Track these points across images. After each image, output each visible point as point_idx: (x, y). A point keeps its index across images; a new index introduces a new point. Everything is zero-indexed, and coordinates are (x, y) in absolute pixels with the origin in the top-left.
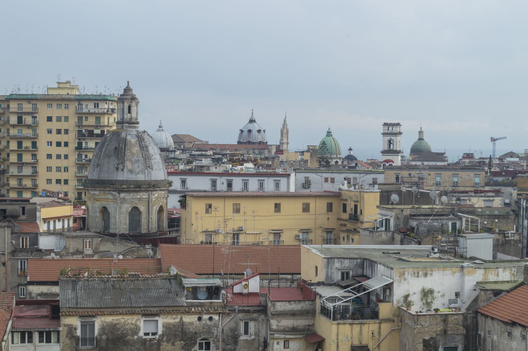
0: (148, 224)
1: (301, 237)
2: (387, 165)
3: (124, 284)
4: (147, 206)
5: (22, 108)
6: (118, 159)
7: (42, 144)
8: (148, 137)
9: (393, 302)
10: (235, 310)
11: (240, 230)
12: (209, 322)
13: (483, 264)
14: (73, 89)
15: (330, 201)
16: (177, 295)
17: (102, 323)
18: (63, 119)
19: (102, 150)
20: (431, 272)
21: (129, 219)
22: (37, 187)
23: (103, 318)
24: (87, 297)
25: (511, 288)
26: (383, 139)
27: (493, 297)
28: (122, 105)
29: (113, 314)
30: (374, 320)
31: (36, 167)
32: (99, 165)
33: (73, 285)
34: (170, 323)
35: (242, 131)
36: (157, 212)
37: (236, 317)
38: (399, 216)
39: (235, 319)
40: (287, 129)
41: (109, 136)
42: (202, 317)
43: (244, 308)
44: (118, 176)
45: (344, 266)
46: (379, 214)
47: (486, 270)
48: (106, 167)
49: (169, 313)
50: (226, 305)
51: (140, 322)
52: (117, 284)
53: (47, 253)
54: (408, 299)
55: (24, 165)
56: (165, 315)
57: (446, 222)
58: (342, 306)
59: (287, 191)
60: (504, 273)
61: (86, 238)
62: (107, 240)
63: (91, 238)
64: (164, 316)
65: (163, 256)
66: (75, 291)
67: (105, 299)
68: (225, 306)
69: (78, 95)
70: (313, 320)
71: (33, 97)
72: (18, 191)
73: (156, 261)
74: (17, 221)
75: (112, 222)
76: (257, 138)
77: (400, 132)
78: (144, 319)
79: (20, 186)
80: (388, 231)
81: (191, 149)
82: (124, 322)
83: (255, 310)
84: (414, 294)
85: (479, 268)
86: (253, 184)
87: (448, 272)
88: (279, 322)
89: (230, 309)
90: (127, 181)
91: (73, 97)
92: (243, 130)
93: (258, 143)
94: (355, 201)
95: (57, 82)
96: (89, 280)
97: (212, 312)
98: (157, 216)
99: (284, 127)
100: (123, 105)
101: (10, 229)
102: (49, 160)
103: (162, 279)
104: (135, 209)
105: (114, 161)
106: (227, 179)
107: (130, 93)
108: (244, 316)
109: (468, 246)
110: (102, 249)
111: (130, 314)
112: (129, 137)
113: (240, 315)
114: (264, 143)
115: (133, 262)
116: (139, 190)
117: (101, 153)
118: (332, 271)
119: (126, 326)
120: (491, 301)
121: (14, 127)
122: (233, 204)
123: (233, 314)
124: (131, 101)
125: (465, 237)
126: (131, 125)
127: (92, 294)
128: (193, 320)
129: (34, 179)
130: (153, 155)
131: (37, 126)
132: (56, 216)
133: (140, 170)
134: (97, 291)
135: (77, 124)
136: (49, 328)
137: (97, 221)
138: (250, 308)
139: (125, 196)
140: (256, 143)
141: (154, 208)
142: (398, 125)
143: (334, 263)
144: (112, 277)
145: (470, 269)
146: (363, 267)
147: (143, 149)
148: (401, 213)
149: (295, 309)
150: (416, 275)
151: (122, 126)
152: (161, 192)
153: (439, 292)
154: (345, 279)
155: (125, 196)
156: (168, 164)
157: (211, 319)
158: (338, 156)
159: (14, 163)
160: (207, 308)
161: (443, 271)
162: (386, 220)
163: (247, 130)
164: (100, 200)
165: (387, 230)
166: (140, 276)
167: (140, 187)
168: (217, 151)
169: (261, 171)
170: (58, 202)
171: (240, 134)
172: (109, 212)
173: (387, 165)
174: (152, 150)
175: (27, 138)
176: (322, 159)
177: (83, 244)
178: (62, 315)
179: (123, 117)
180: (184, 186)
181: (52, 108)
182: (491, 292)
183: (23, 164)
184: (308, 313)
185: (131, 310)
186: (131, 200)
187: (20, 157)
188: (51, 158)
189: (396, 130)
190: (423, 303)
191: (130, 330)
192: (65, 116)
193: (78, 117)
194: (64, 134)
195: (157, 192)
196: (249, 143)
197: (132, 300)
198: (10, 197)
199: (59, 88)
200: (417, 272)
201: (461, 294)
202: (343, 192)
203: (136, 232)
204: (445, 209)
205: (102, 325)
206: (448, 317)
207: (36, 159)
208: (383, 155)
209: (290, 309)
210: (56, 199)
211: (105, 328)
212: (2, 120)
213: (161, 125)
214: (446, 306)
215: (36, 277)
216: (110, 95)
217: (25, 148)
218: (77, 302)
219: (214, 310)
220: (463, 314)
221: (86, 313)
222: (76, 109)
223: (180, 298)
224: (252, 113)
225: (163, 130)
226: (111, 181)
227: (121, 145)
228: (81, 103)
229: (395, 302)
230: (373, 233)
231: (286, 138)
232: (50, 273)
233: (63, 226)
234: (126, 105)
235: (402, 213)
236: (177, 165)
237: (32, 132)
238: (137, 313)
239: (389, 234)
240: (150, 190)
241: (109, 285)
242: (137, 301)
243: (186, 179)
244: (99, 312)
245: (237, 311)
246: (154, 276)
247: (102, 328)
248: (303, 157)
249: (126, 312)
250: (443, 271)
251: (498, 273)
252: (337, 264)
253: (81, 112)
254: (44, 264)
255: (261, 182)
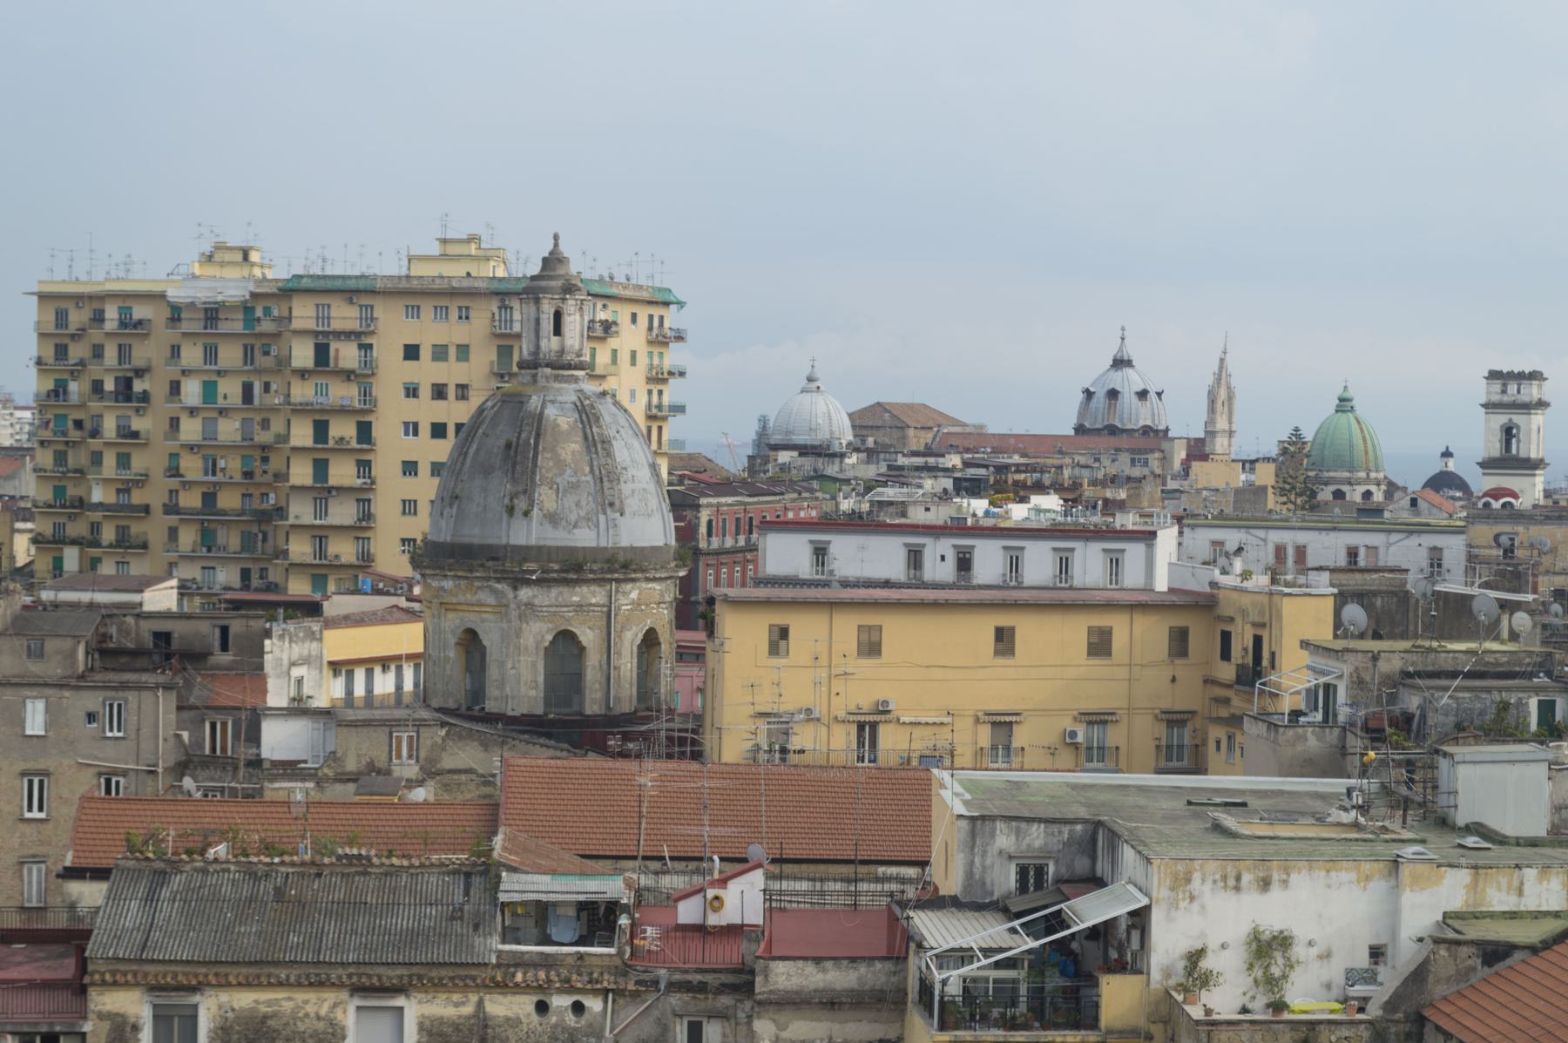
0: (604, 684)
1: (1080, 738)
2: (1496, 505)
3: (316, 887)
4: (605, 631)
5: (329, 318)
6: (514, 480)
7: (386, 430)
8: (614, 410)
9: (1148, 974)
10: (656, 982)
11: (882, 709)
12: (570, 1019)
13: (1489, 849)
14: (488, 259)
15: (1179, 621)
16: (476, 927)
17: (222, 1012)
18: (452, 352)
19: (468, 449)
20: (1284, 877)
21: (545, 671)
22: (373, 561)
23: (224, 997)
24: (185, 925)
25: (1544, 937)
26: (1487, 421)
27: (1480, 967)
28: (533, 308)
29: (256, 985)
30: (1083, 1032)
31: (369, 501)
32: (456, 497)
33: (154, 885)
34: (442, 1018)
35: (1089, 394)
36: (635, 649)
37: (660, 1006)
38: (1363, 675)
39: (656, 1013)
40: (1229, 388)
41: (493, 407)
42: (548, 1001)
43: (689, 977)
44: (511, 533)
45: (1029, 846)
46: (1309, 667)
47: (1477, 874)
48: (478, 504)
49: (438, 986)
50: (630, 966)
51: (345, 1012)
52: (294, 886)
53: (275, 772)
54: (1200, 964)
55: (334, 493)
56: (426, 992)
57: (1520, 699)
58: (995, 981)
59: (1146, 584)
60: (1545, 883)
61: (398, 728)
62: (464, 734)
63: (415, 729)
64: (423, 996)
65: (510, 795)
66: (150, 907)
67: (239, 931)
68: (624, 970)
69: (501, 279)
70: (898, 1025)
71: (361, 284)
72: (313, 575)
73: (484, 812)
74: (206, 669)
75: (494, 678)
76: (1137, 415)
77: (1540, 399)
78: (357, 1001)
79: (320, 559)
80: (1330, 724)
81: (892, 450)
82: (292, 1012)
83: (723, 985)
84: (1223, 946)
85: (1451, 866)
86: (1039, 563)
87: (1345, 875)
88: (782, 1027)
89: (641, 978)
90: (540, 548)
91: (482, 285)
92: (1092, 389)
93: (1138, 430)
94: (1254, 625)
95: (437, 239)
96: (208, 871)
97: (579, 985)
98: (635, 660)
99: (1219, 383)
100: (538, 309)
101: (173, 696)
102: (409, 480)
103: (444, 873)
104: (566, 639)
105: (501, 486)
106: (955, 546)
107: (561, 271)
108: (686, 1003)
109: (1460, 787)
110: (448, 762)
111: (311, 984)
112: (551, 412)
113: (675, 1000)
114: (1157, 432)
115: (412, 811)
116: (575, 577)
117: (464, 459)
118: (988, 862)
119: (299, 1023)
120: (1473, 980)
121: (303, 376)
122: (859, 626)
123: (652, 994)
124: (562, 296)
125: (1452, 755)
126: (562, 372)
127: (203, 917)
128: (520, 1011)
129: (363, 538)
130: (625, 469)
131: (373, 374)
132: (379, 655)
133: (582, 513)
134: (222, 908)
135: (496, 368)
136: (51, 1024)
137: (448, 672)
138: (708, 978)
139: (534, 596)
140: (1133, 430)
141: (628, 635)
142: (1535, 376)
143: (993, 835)
144: (282, 863)
145: (1420, 868)
146: (1094, 850)
147: (593, 450)
148: (1370, 665)
149: (838, 987)
150: (1231, 882)
151: (535, 376)
152: (650, 585)
153: (1310, 944)
154: (1032, 889)
155: (534, 596)
156: (800, 494)
157: (578, 1008)
158: (1373, 475)
159: (302, 489)
160: (564, 972)
161: (1328, 871)
162: (1327, 687)
163: (1105, 389)
164: (458, 607)
165: (1327, 722)
166: (375, 860)
167: (579, 568)
168: (976, 456)
169: (1082, 520)
170: (407, 611)
171: (1081, 403)
172: (485, 647)
173: (1496, 505)
174: (625, 450)
175: (343, 411)
176: (1289, 484)
177: (391, 746)
178: (93, 984)
179: (538, 347)
180: (823, 564)
181: (418, 317)
182: (1473, 950)
183: (330, 490)
184: (879, 1000)
185: (316, 971)
186: (552, 609)
187: (321, 468)
188: (416, 474)
189: (1532, 392)
190: (1256, 981)
191: (311, 1036)
192: (459, 343)
193: (498, 346)
194: (457, 399)
195: (638, 584)
196: (1112, 430)
197: (324, 939)
198: (290, 592)
199: (444, 257)
200: (1234, 874)
201: (1389, 952)
202: (1221, 594)
203: (567, 711)
204: (1523, 655)
205: (221, 1016)
206: (1320, 1032)
207: (370, 477)
208: (1484, 474)
209: (821, 985)
210: (402, 602)
211: (231, 1026)
212: (273, 354)
213: (812, 372)
214: (1336, 992)
215: (95, 855)
216: (601, 280)
217: (337, 442)
218: (147, 940)
219: (586, 978)
220: (1370, 1022)
221: (169, 979)
222: (494, 321)
223: (485, 936)
224: (1123, 339)
225: (818, 388)
226: (490, 547)
227: (523, 436)
228: (507, 303)
229: (1156, 975)
230: (1277, 731)
231: (1225, 417)
232: (337, 825)
233: (399, 687)
234: (548, 309)
235: (1375, 666)
236: (834, 498)
237: (357, 393)
238: (333, 984)
239: (1331, 734)
240: (613, 580)
241: (265, 888)
242: (338, 944)
243: (829, 542)
244: (211, 977)
245: (663, 988)
246: (417, 864)
247: (222, 1028)
248: (1252, 477)
249: (299, 976)
250: (1328, 871)
251: (1522, 883)
252: (1004, 839)
253: (508, 331)
254: (128, 812)
255: (1064, 555)
